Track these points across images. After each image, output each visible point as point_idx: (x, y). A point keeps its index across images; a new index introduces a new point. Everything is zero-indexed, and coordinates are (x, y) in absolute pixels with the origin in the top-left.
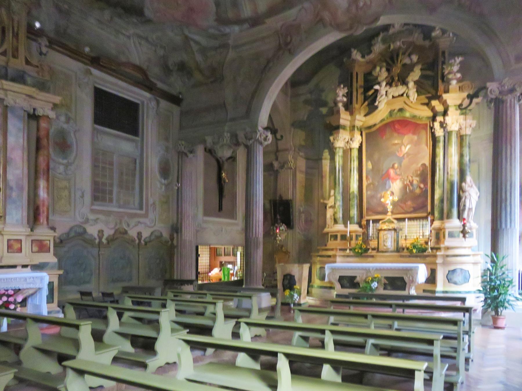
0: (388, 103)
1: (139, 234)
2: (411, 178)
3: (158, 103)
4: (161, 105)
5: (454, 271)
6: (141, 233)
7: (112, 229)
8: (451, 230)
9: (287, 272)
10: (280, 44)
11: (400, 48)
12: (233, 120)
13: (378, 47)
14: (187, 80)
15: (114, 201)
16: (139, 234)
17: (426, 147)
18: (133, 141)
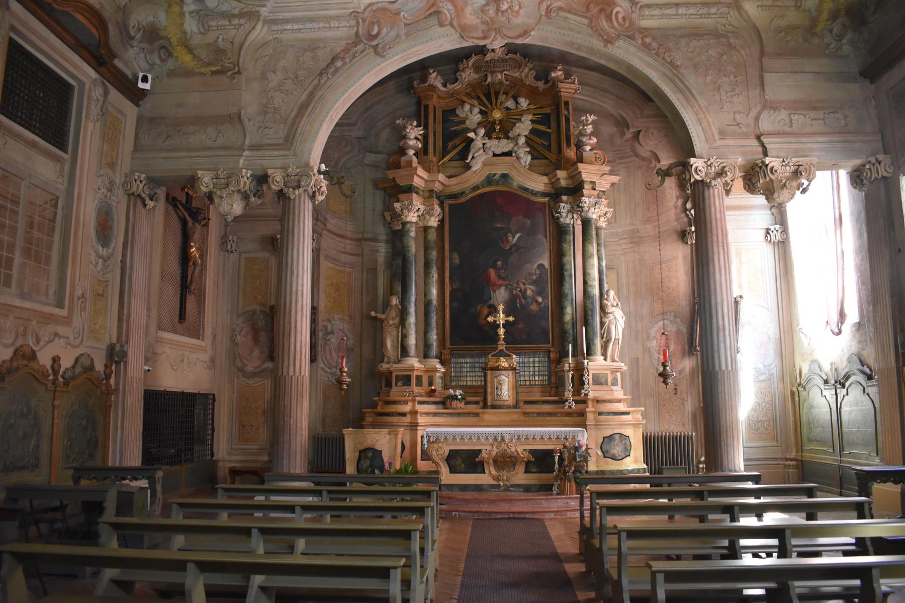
0: (485, 164)
1: (56, 360)
2: (522, 285)
3: (106, 93)
4: (110, 98)
5: (610, 438)
6: (59, 358)
7: (7, 346)
8: (594, 372)
9: (368, 443)
10: (357, 34)
11: (501, 83)
12: (254, 148)
13: (468, 75)
14: (158, 61)
15: (14, 283)
16: (56, 360)
17: (544, 240)
18: (58, 159)
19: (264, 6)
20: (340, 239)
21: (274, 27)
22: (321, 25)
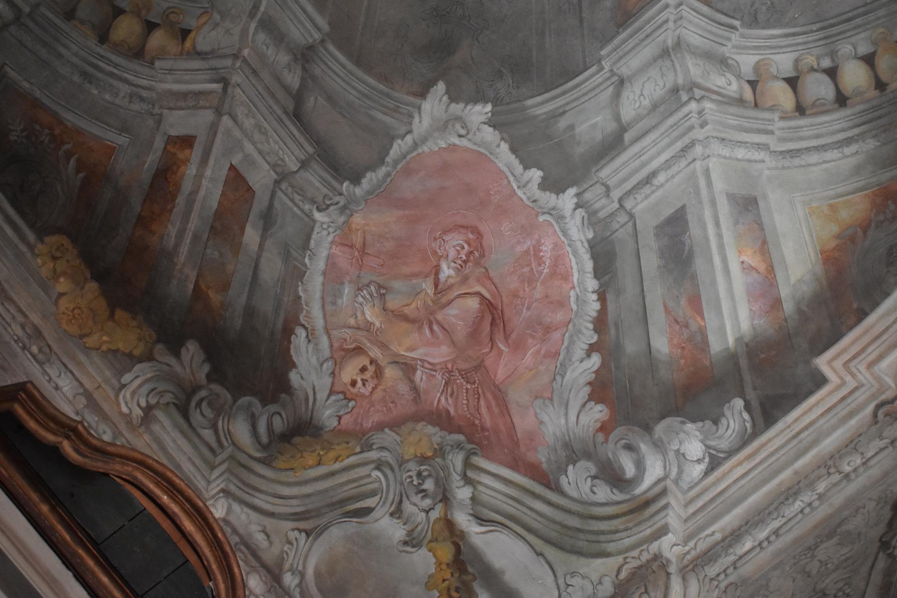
19: (664, 531)
20: (649, 40)
21: (712, 570)
22: (821, 487)
